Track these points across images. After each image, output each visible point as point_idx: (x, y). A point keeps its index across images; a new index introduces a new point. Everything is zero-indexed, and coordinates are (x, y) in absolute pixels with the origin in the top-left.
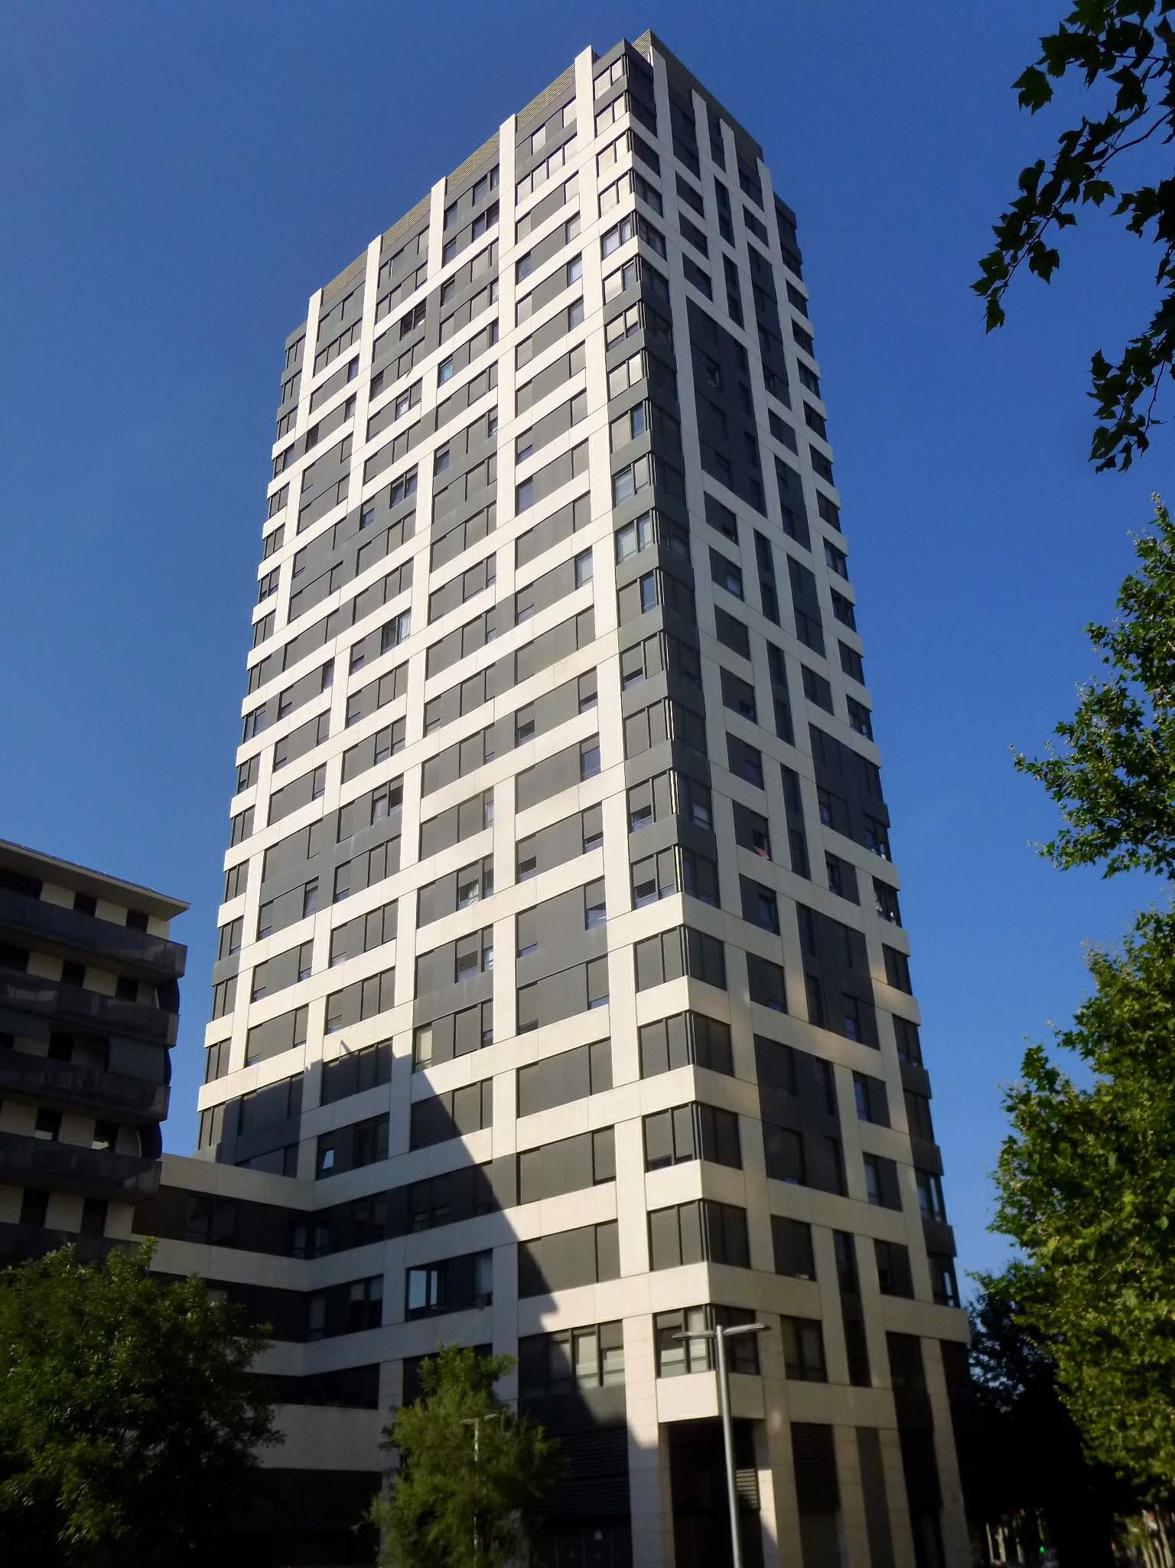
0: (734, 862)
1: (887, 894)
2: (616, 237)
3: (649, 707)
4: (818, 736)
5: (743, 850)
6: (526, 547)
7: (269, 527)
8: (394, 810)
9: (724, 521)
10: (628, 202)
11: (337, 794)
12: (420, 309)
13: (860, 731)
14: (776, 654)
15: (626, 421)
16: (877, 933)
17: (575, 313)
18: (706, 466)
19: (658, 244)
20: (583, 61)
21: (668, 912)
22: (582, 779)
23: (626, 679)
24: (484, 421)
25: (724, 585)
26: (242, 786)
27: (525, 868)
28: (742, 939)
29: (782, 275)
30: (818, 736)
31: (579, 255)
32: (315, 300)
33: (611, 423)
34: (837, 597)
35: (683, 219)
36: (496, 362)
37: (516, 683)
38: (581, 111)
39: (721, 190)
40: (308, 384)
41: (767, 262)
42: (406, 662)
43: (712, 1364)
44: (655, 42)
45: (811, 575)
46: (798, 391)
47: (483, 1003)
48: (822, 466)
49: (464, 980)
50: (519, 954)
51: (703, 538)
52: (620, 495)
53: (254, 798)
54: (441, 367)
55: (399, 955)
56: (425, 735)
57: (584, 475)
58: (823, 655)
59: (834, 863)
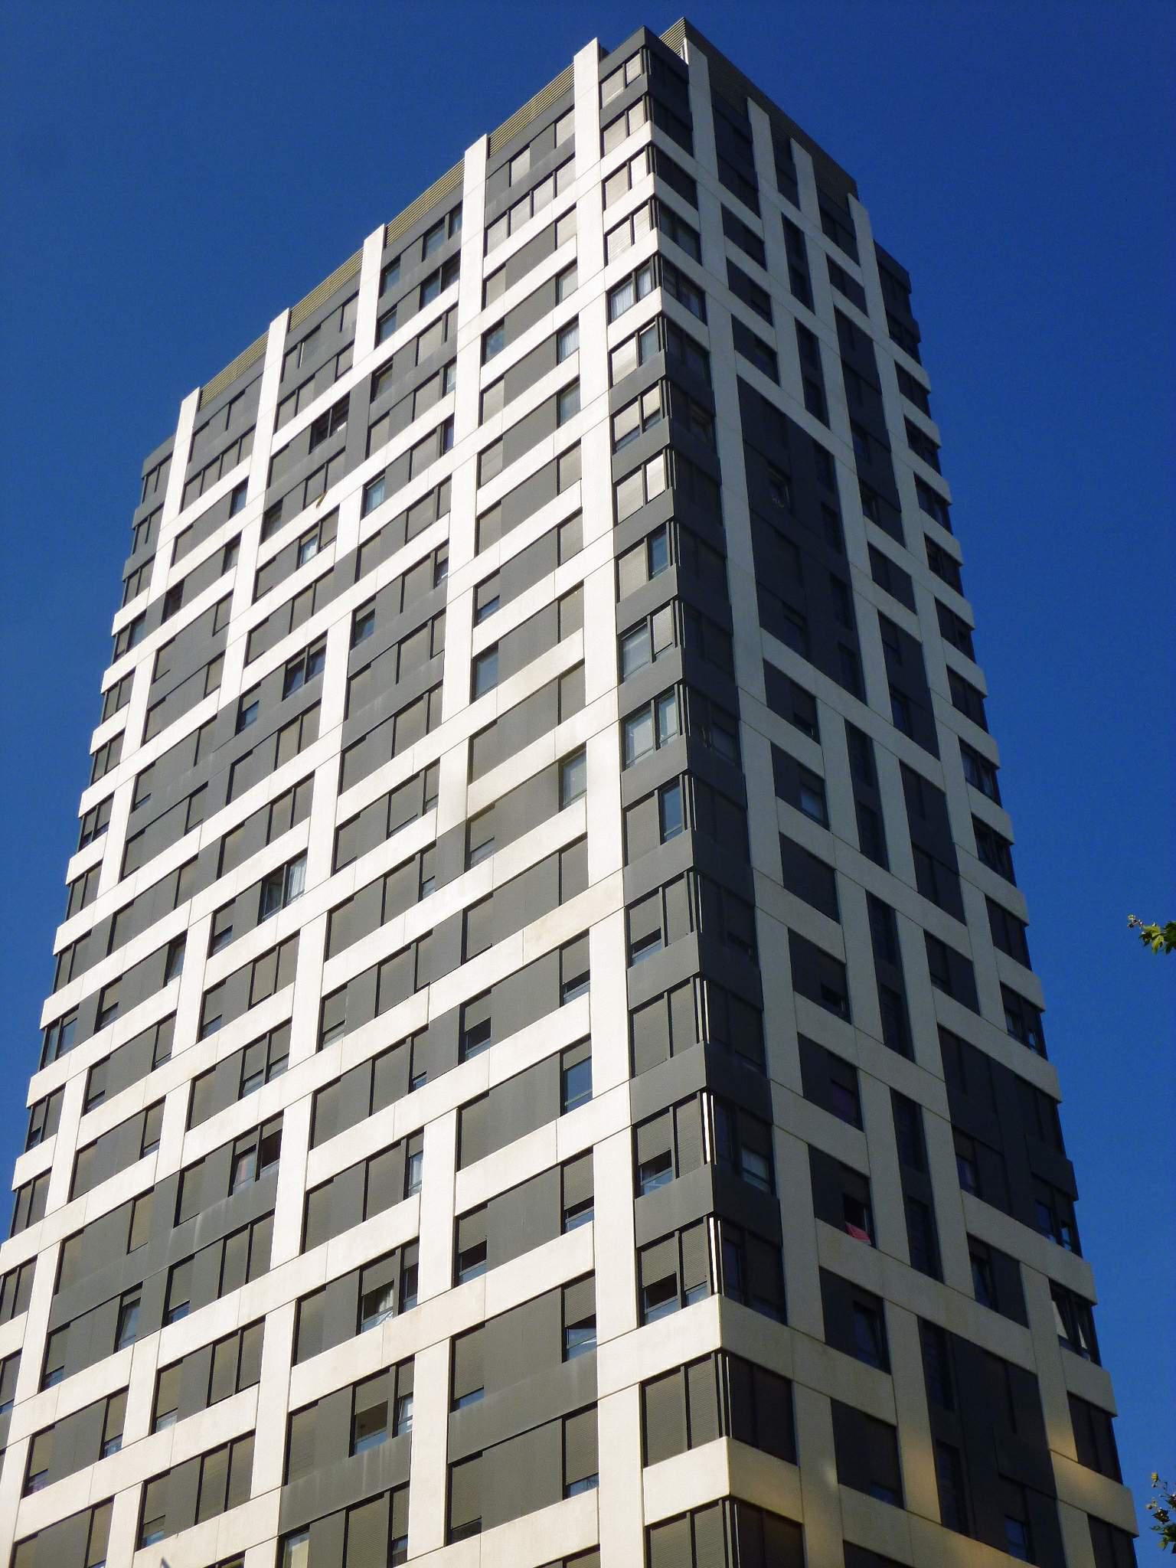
0: (809, 1245)
1: (1075, 1308)
2: (630, 292)
3: (671, 991)
4: (952, 1044)
5: (826, 1229)
6: (485, 748)
7: (100, 736)
8: (265, 1172)
9: (800, 710)
10: (648, 241)
11: (179, 1147)
12: (340, 410)
13: (1025, 1041)
14: (881, 915)
15: (640, 555)
16: (1058, 1377)
17: (568, 401)
18: (767, 621)
19: (694, 301)
20: (586, 62)
21: (697, 1328)
22: (564, 1111)
23: (634, 949)
24: (430, 563)
25: (796, 804)
26: (35, 1137)
27: (468, 1260)
28: (823, 1379)
29: (888, 355)
30: (952, 1044)
31: (576, 319)
32: (189, 406)
33: (618, 558)
34: (982, 829)
35: (738, 326)
36: (449, 478)
37: (464, 960)
38: (583, 124)
39: (794, 236)
40: (172, 522)
41: (865, 335)
42: (296, 934)
43: (728, 1434)
44: (692, 33)
45: (940, 795)
46: (915, 519)
47: (394, 1490)
48: (956, 631)
49: (364, 1453)
50: (454, 1404)
51: (761, 731)
52: (630, 667)
53: (51, 1157)
54: (368, 489)
55: (260, 1412)
56: (320, 1048)
57: (577, 636)
58: (962, 919)
59: (982, 1255)
